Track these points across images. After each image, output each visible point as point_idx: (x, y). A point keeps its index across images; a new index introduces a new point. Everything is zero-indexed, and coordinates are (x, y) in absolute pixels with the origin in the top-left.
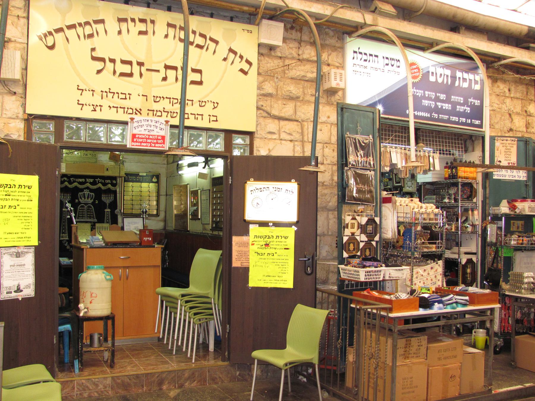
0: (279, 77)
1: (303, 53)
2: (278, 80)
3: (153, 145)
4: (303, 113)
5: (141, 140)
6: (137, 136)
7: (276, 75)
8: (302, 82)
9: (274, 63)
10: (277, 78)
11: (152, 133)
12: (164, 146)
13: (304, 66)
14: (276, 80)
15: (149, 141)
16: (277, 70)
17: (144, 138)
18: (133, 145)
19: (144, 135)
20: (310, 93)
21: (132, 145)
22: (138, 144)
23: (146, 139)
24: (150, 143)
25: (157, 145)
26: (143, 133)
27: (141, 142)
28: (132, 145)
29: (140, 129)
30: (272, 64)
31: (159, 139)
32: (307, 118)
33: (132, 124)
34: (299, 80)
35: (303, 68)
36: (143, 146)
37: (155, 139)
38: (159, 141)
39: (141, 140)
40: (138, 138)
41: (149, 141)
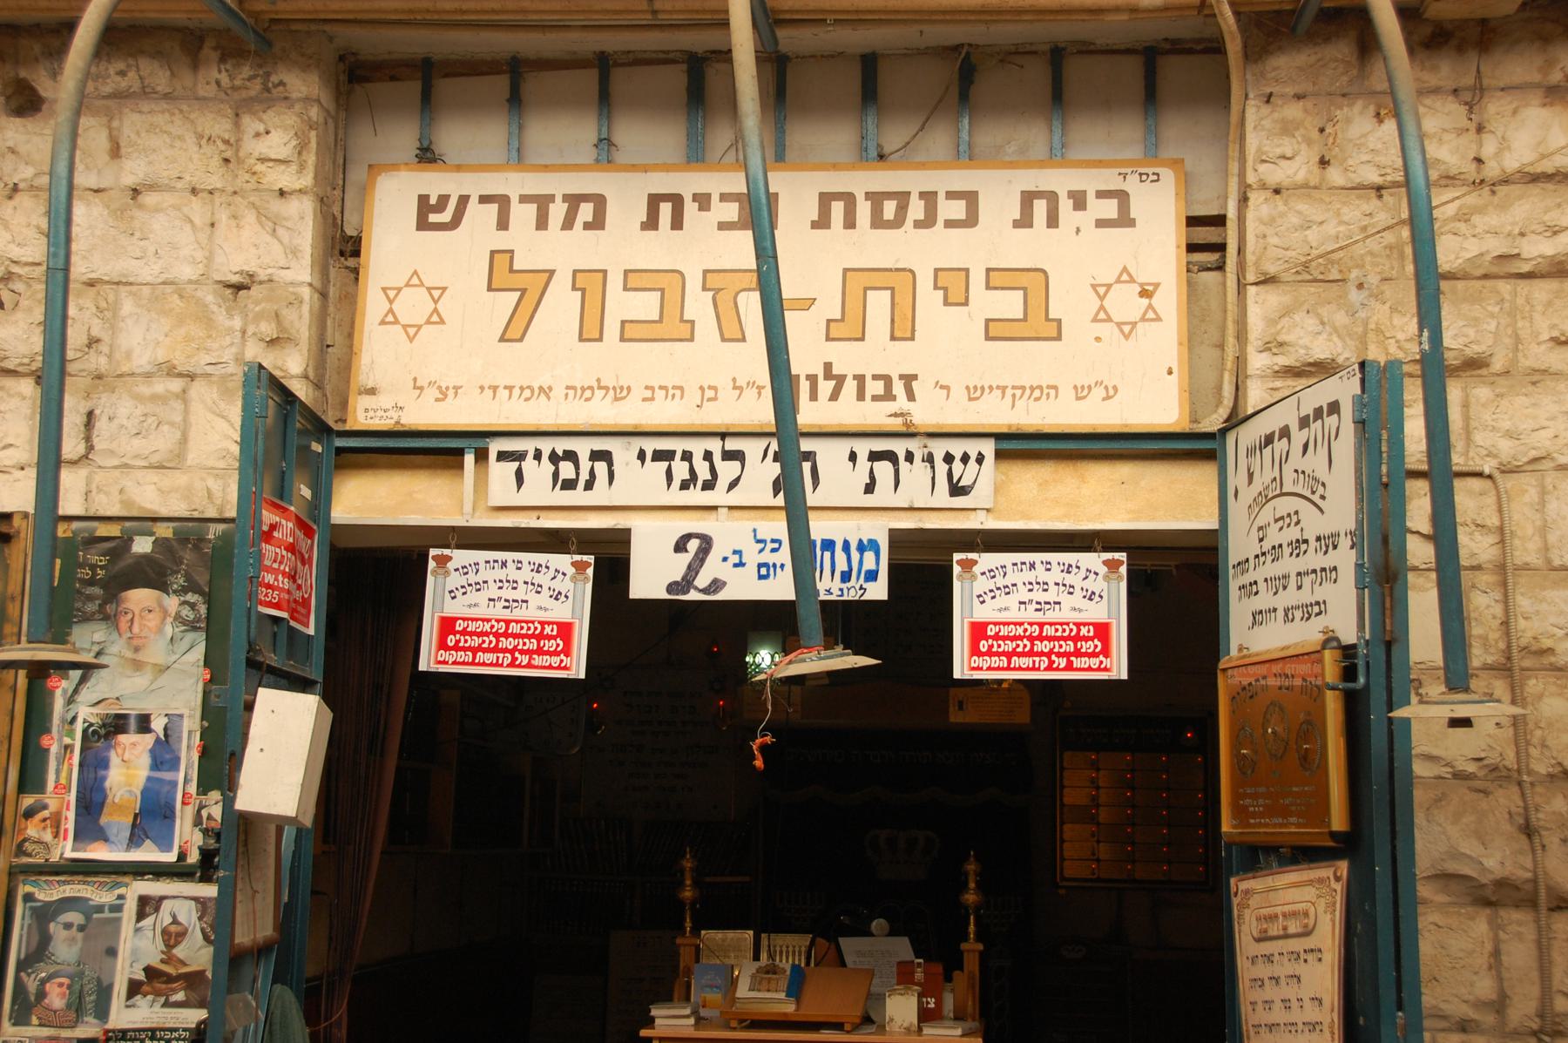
0: (1373, 279)
1: (1504, 145)
2: (1365, 293)
3: (525, 660)
4: (1509, 435)
5: (476, 641)
6: (460, 626)
7: (1354, 274)
8: (1505, 287)
9: (1341, 223)
10: (1360, 286)
11: (519, 613)
12: (1106, 662)
13: (1503, 207)
14: (1355, 296)
15: (506, 643)
16: (1359, 250)
17: (1020, 638)
18: (979, 668)
19: (488, 620)
20: (1546, 336)
21: (973, 669)
22: (461, 656)
23: (1031, 639)
24: (512, 652)
25: (537, 660)
26: (1014, 614)
27: (475, 650)
28: (973, 669)
29: (1002, 600)
30: (1331, 228)
31: (549, 638)
32: (1533, 454)
33: (440, 579)
34: (1486, 277)
35: (1492, 219)
36: (484, 664)
37: (1065, 639)
38: (549, 645)
39: (476, 641)
40: (464, 632)
41: (506, 643)
